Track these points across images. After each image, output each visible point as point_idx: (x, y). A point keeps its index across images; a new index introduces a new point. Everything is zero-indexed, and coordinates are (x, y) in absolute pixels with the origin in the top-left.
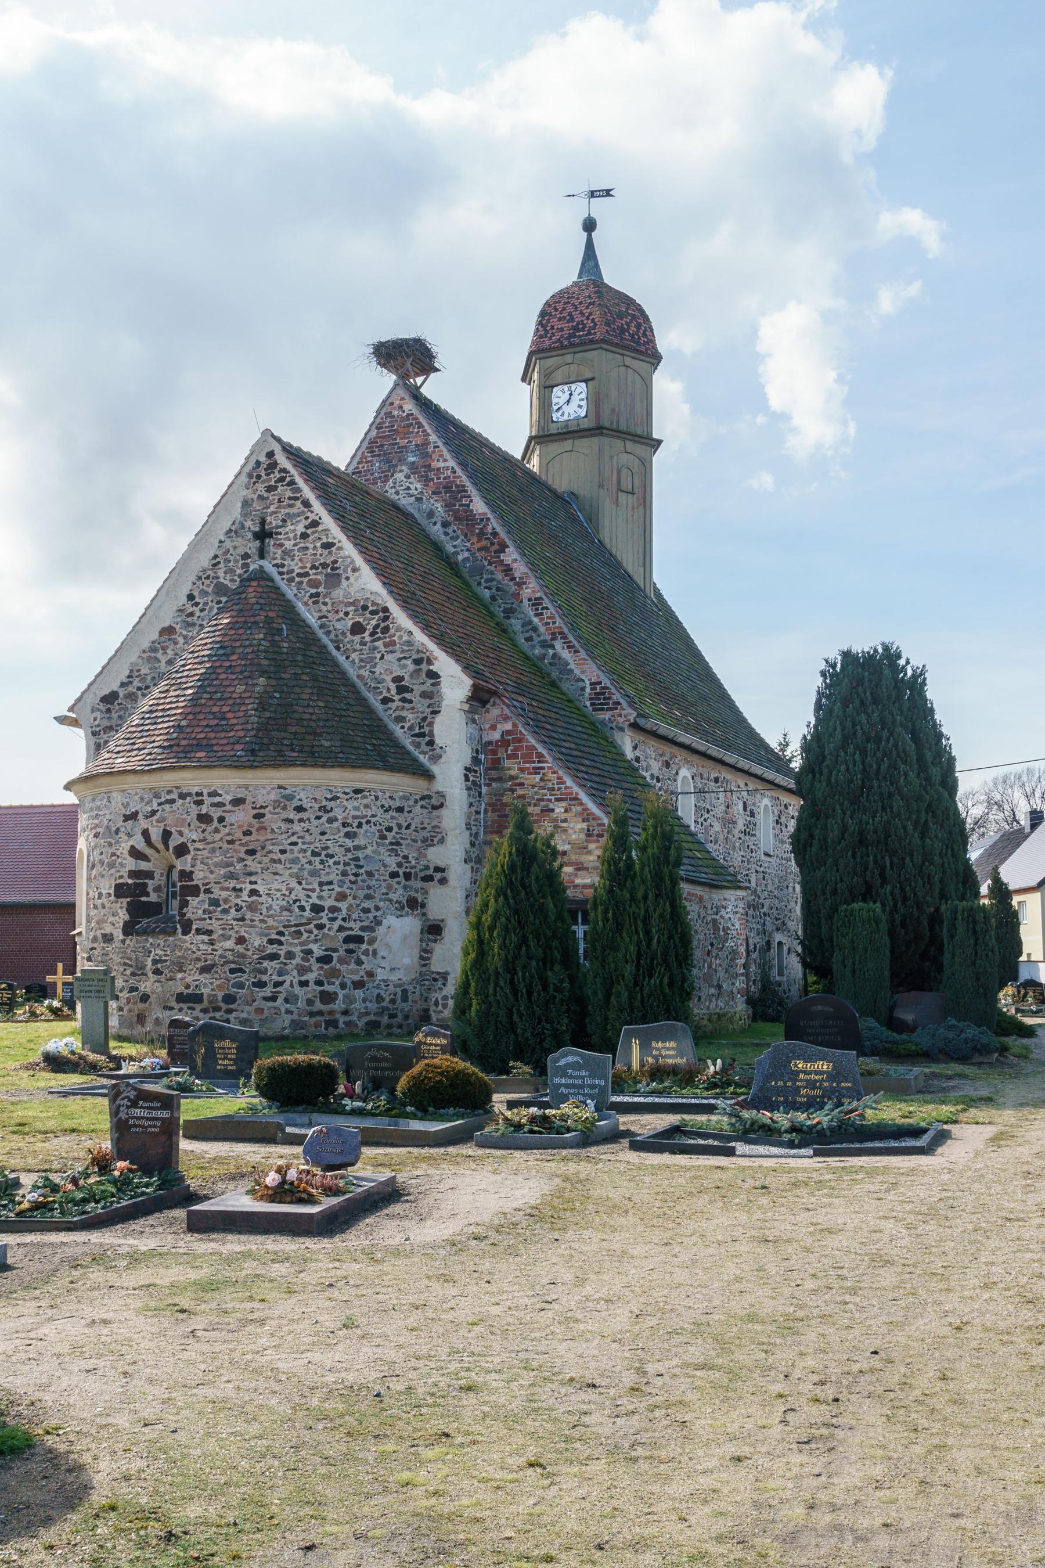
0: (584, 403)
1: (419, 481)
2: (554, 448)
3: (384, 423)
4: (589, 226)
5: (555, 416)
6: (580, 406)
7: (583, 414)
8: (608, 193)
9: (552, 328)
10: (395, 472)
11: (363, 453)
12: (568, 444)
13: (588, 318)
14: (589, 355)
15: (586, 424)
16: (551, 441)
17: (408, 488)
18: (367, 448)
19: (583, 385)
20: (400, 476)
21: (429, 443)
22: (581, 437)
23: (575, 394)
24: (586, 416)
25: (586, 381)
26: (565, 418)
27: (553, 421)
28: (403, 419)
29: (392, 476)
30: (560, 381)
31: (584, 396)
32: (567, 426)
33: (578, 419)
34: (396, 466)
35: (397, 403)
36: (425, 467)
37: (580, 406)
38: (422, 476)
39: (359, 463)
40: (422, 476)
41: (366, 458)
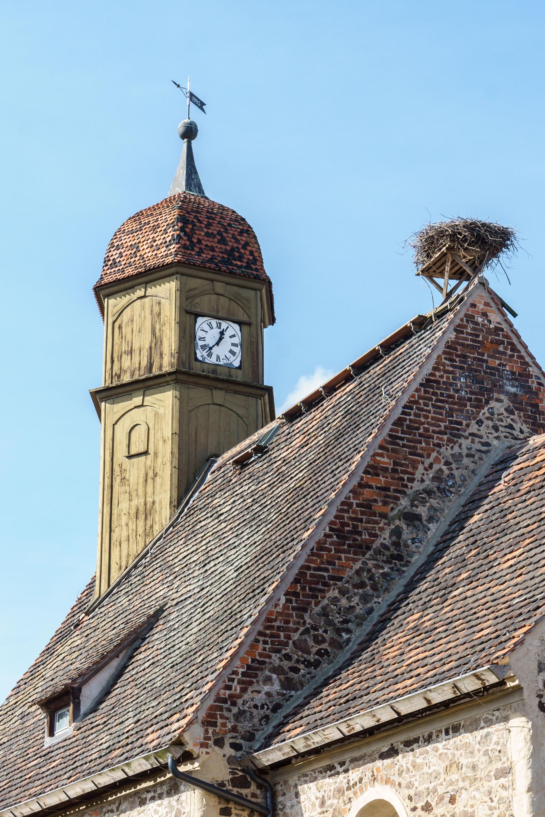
0: (237, 350)
1: (526, 422)
2: (200, 395)
3: (466, 327)
4: (190, 133)
5: (200, 354)
6: (233, 353)
7: (237, 364)
8: (201, 105)
9: (199, 242)
10: (491, 398)
11: (439, 357)
12: (219, 396)
13: (244, 247)
14: (245, 293)
15: (239, 377)
16: (196, 384)
17: (511, 427)
18: (444, 353)
19: (237, 327)
20: (499, 407)
21: (530, 376)
22: (236, 392)
23: (227, 334)
24: (240, 368)
25: (240, 323)
26: (213, 360)
27: (196, 359)
28: (489, 331)
29: (487, 403)
30: (206, 311)
31: (237, 340)
32: (214, 372)
33: (229, 367)
34: (490, 391)
35: (481, 306)
36: (532, 405)
37: (233, 353)
38: (529, 417)
39: (434, 369)
40: (529, 417)
41: (444, 365)
